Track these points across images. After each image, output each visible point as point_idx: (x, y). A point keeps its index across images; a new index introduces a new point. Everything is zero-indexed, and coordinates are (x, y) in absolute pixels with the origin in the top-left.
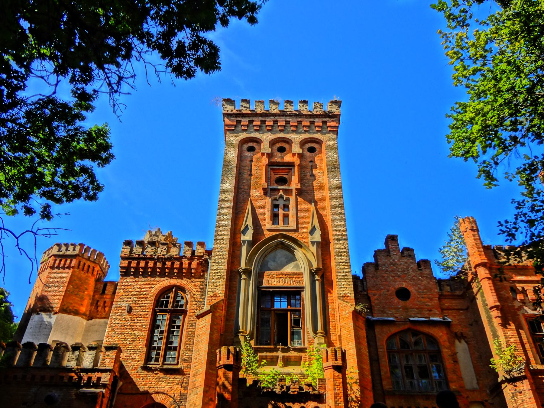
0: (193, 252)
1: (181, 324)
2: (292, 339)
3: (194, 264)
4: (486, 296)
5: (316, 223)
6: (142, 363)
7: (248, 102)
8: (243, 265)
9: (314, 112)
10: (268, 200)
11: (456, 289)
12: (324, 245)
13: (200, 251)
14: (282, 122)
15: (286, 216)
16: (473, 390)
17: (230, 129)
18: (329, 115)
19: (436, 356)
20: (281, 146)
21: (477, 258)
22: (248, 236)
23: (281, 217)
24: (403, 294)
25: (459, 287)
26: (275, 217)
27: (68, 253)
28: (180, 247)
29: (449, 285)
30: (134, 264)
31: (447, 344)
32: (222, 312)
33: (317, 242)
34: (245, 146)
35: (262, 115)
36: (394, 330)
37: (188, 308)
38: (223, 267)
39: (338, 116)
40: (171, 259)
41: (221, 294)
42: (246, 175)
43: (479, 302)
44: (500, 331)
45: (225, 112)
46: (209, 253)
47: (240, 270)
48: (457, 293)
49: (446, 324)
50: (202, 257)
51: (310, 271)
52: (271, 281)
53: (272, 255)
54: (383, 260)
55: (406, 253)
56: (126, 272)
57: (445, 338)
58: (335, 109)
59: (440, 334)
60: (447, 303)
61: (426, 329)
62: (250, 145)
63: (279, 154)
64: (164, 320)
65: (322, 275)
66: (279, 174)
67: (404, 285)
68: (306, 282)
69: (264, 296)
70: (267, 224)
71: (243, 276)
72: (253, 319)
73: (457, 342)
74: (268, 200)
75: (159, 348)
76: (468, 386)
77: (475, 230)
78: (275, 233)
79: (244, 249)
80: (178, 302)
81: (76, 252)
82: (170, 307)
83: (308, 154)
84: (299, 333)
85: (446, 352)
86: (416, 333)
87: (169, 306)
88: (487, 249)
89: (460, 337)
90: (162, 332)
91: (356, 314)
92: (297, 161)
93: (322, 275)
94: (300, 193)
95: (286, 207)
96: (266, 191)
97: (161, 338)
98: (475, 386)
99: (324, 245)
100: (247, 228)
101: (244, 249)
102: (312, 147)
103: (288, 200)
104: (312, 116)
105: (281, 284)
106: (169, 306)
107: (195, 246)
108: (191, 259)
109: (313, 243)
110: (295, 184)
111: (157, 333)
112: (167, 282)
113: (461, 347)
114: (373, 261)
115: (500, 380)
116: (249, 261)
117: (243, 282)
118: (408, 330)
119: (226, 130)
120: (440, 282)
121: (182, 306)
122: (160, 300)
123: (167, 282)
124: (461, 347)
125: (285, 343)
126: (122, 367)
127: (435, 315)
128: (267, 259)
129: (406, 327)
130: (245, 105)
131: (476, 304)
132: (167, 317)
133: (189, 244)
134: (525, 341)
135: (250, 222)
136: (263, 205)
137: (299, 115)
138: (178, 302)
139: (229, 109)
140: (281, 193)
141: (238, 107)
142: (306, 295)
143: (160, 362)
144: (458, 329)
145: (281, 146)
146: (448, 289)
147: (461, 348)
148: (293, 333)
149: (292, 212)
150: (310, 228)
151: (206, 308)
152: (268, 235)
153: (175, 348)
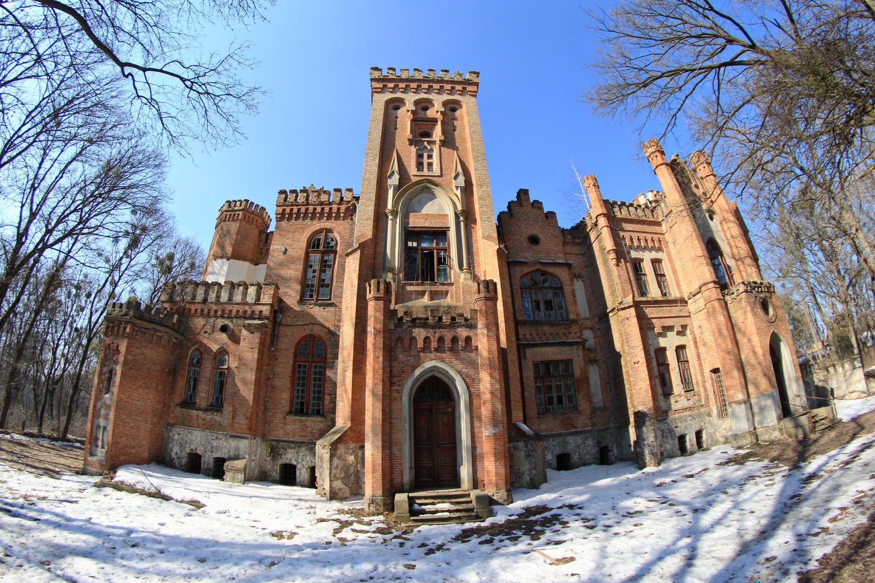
0: (342, 198)
1: (332, 263)
2: (439, 276)
3: (343, 208)
4: (602, 242)
5: (460, 169)
6: (298, 298)
7: (394, 70)
8: (390, 206)
9: (456, 79)
10: (413, 149)
11: (575, 238)
12: (467, 190)
13: (347, 196)
14: (425, 86)
15: (430, 165)
16: (586, 319)
17: (374, 91)
18: (469, 82)
19: (559, 290)
20: (423, 105)
21: (597, 209)
22: (394, 180)
23: (425, 166)
24: (534, 240)
25: (579, 234)
26: (420, 165)
27: (236, 208)
28: (329, 194)
29: (571, 234)
30: (288, 210)
31: (569, 282)
32: (369, 251)
33: (461, 187)
34: (391, 106)
35: (406, 80)
36: (526, 270)
37: (338, 249)
38: (371, 208)
39: (477, 84)
40: (321, 203)
41: (369, 235)
42: (392, 129)
43: (596, 247)
44: (614, 270)
45: (373, 77)
46: (357, 199)
47: (387, 211)
48: (577, 241)
49: (569, 266)
50: (349, 202)
51: (456, 214)
52: (416, 221)
53: (418, 198)
54: (516, 210)
55: (536, 205)
56: (281, 217)
57: (568, 277)
58: (474, 78)
59: (563, 274)
60: (569, 249)
61: (551, 270)
62: (394, 105)
63: (423, 112)
64: (316, 258)
65: (467, 216)
66: (421, 130)
67: (535, 232)
68: (451, 223)
69: (409, 234)
70: (412, 170)
71: (390, 217)
72: (400, 256)
73: (575, 280)
74: (413, 149)
75: (313, 286)
76: (582, 316)
77: (596, 186)
78: (421, 178)
79: (391, 192)
80: (329, 243)
81: (242, 207)
82: (321, 248)
83: (450, 113)
84: (445, 270)
85: (567, 289)
86: (544, 273)
87: (321, 248)
88: (606, 203)
89: (578, 276)
90: (314, 271)
91: (499, 251)
92: (439, 116)
93: (467, 216)
94: (444, 144)
95: (430, 157)
96: (411, 142)
97: (314, 277)
98: (587, 315)
99: (467, 190)
100: (393, 172)
101: (391, 192)
102: (452, 107)
103: (432, 150)
104: (452, 82)
105: (427, 225)
106: (321, 248)
107: (343, 191)
108: (340, 204)
109: (457, 187)
110: (437, 133)
111: (310, 271)
112: (317, 225)
113: (579, 285)
114: (515, 200)
115: (608, 311)
116: (395, 203)
117: (390, 222)
118: (538, 270)
119: (373, 92)
120: (563, 231)
121: (332, 247)
122: (313, 244)
123: (317, 225)
124: (579, 285)
125: (432, 279)
126: (280, 301)
127: (560, 258)
128: (414, 201)
129: (536, 268)
130: (391, 72)
131: (592, 250)
132: (319, 256)
133: (338, 190)
134: (632, 278)
135: (396, 168)
136: (410, 155)
137: (441, 81)
138: (329, 243)
139: (376, 74)
140: (426, 143)
141: (385, 73)
142: (452, 234)
143: (315, 297)
144: (577, 271)
145: (423, 105)
146: (570, 237)
147: (579, 286)
148: (439, 270)
149: (435, 160)
150: (453, 175)
151: (356, 245)
152: (414, 179)
153: (327, 286)
